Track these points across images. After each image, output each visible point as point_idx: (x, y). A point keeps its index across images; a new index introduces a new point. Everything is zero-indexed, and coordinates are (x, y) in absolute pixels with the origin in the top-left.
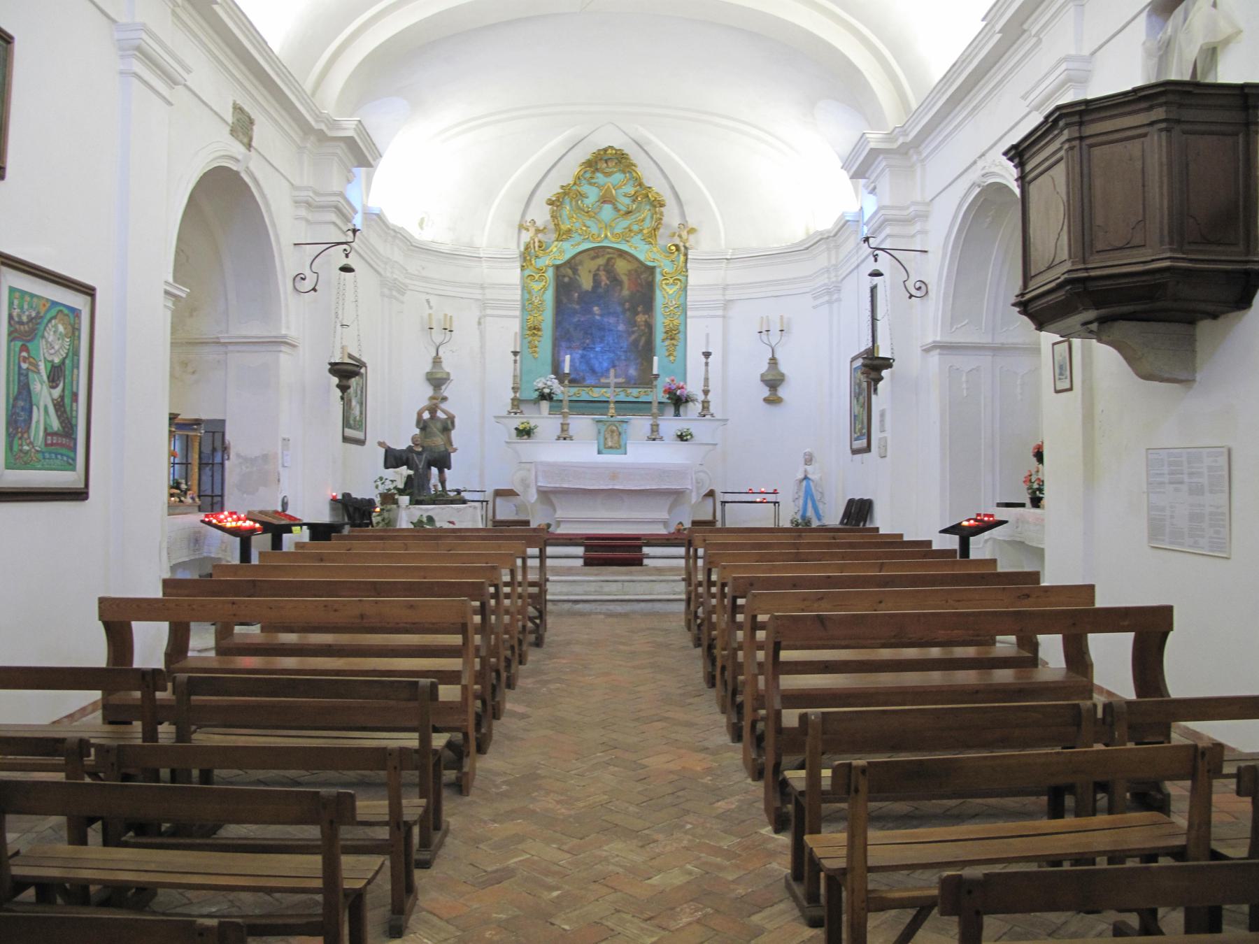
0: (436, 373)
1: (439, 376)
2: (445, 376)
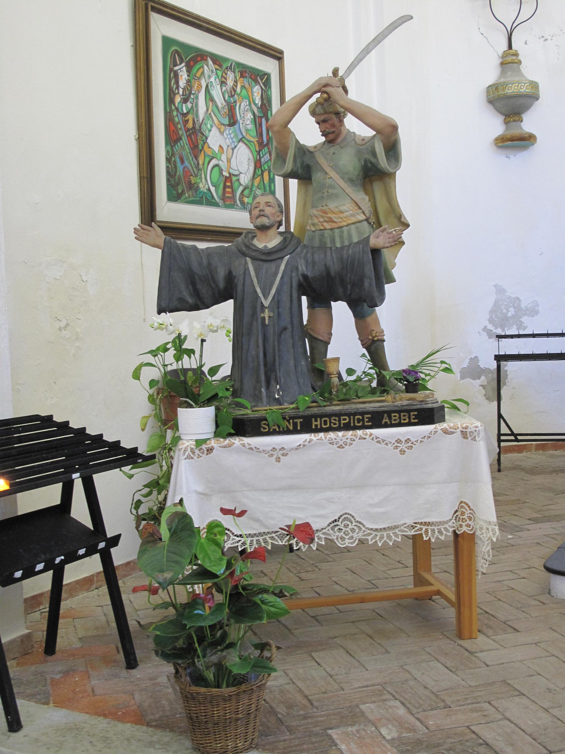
0: (505, 85)
1: (511, 90)
2: (524, 89)
